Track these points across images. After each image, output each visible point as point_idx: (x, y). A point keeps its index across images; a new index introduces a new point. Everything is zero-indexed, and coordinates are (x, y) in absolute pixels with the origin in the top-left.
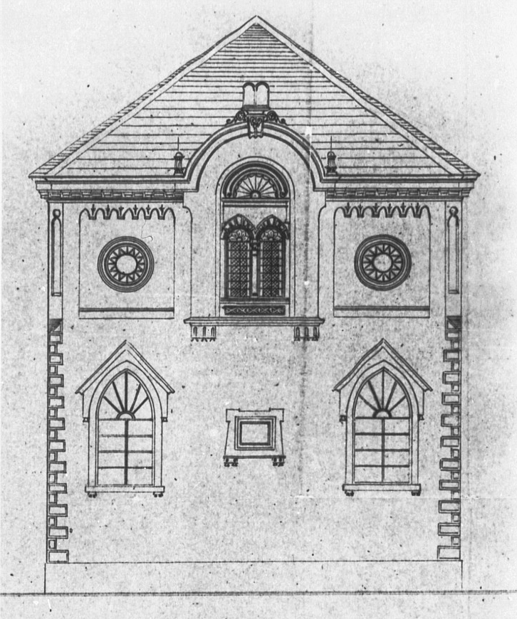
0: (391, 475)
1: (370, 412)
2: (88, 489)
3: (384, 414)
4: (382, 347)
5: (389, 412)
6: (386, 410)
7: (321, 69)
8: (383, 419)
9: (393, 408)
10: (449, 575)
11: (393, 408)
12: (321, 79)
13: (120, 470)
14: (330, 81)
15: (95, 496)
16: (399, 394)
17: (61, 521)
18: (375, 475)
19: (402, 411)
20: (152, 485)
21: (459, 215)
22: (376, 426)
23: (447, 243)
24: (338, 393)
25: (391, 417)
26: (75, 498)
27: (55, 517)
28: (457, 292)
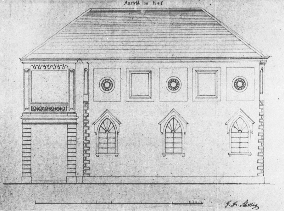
0: (176, 151)
1: (170, 131)
2: (96, 154)
3: (107, 132)
4: (174, 111)
5: (109, 131)
6: (174, 131)
7: (209, 14)
8: (107, 133)
9: (110, 130)
10: (260, 179)
11: (110, 130)
12: (209, 18)
13: (168, 147)
14: (212, 18)
15: (98, 156)
16: (112, 125)
17: (88, 165)
18: (238, 150)
19: (112, 131)
20: (115, 153)
21: (263, 70)
22: (105, 135)
23: (86, 78)
24: (160, 125)
25: (109, 133)
26: (93, 158)
27: (86, 164)
28: (87, 94)
